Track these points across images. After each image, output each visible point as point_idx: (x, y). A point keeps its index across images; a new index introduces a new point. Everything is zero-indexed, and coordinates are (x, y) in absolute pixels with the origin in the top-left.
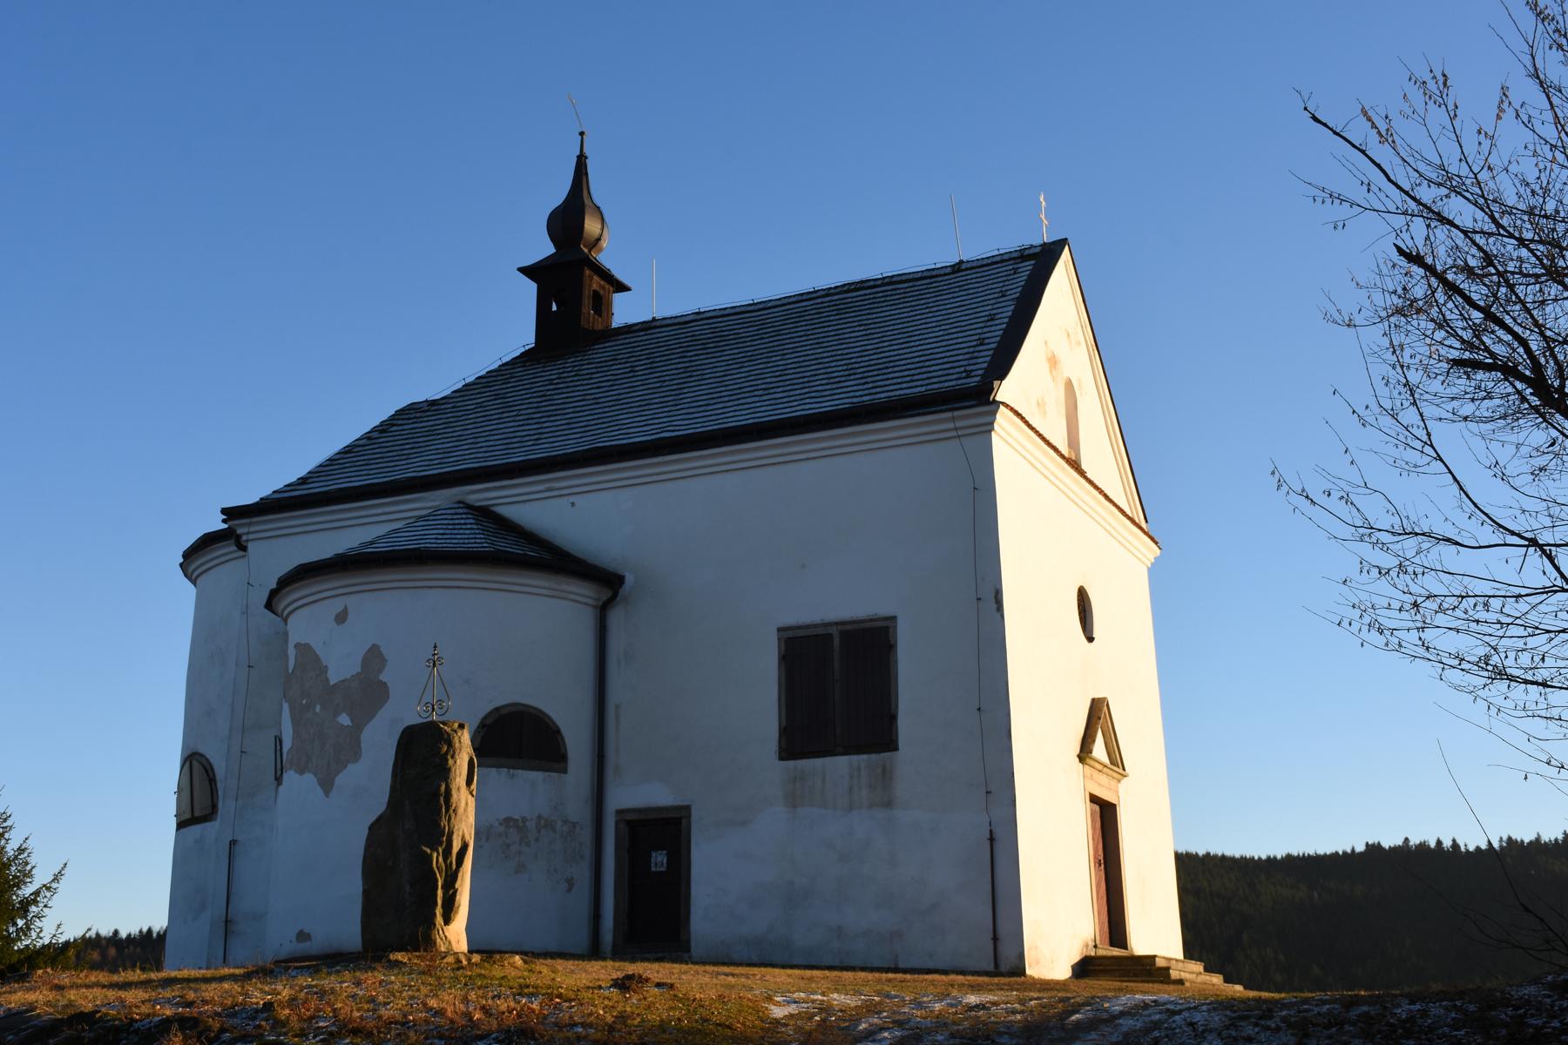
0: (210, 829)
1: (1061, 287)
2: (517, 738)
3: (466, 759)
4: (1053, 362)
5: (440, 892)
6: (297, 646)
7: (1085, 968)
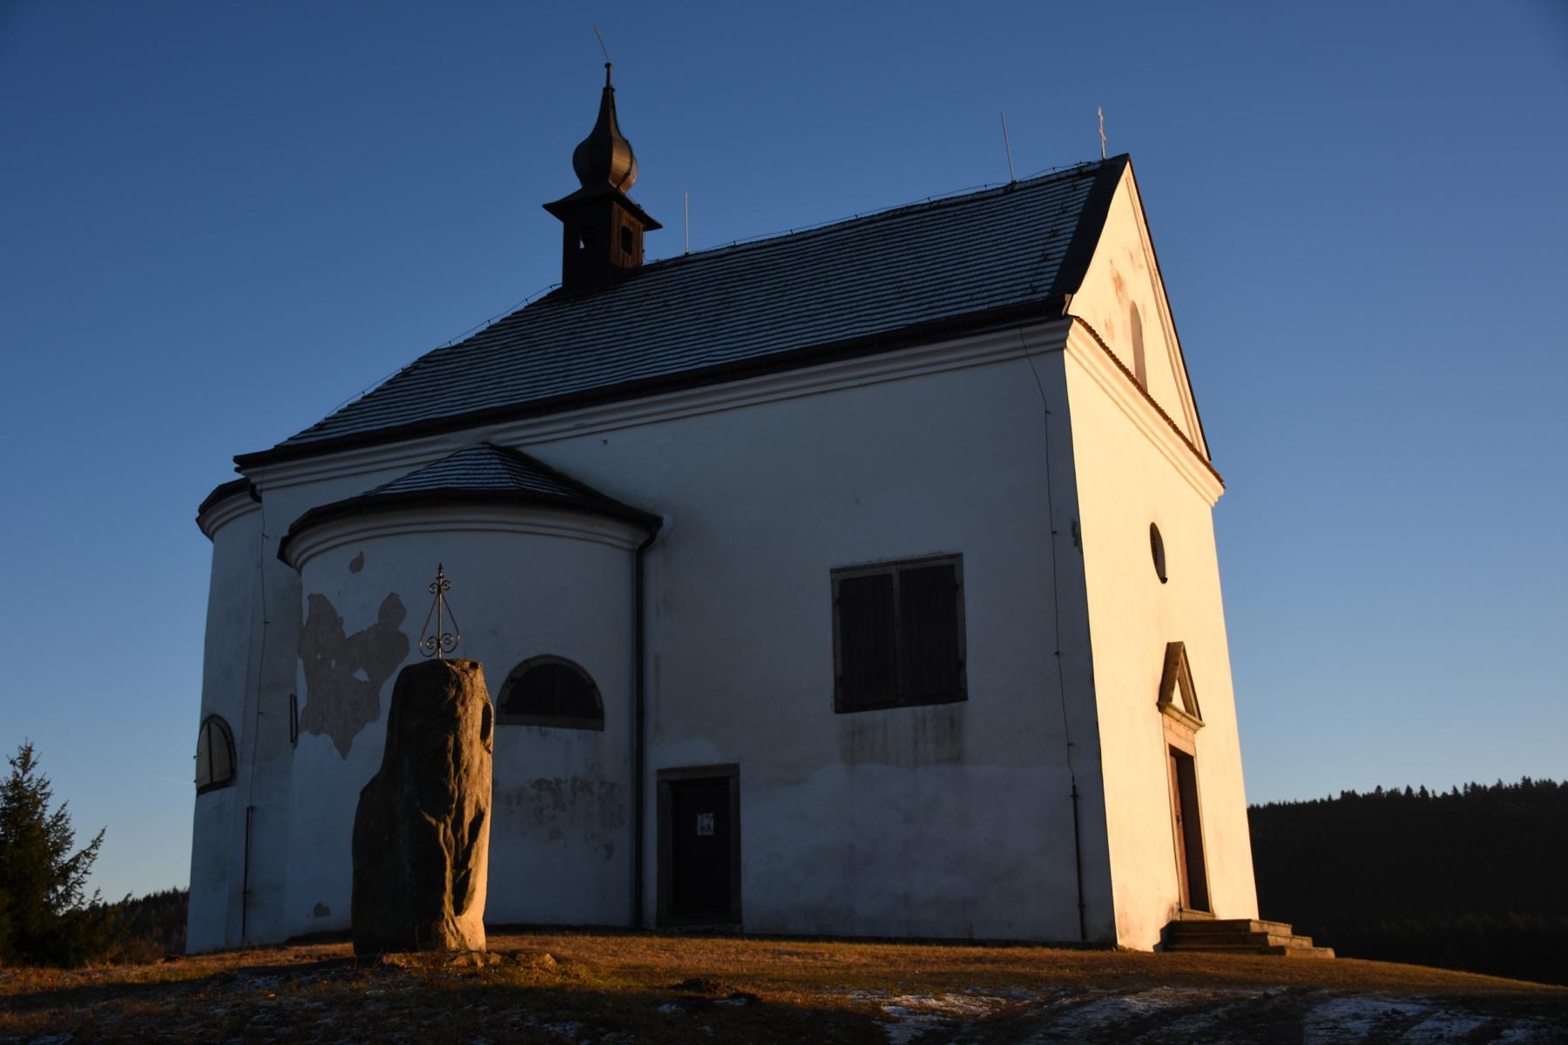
0: (227, 795)
1: (1123, 202)
2: (545, 693)
3: (480, 706)
4: (1119, 282)
5: (449, 874)
6: (311, 597)
7: (1173, 934)
